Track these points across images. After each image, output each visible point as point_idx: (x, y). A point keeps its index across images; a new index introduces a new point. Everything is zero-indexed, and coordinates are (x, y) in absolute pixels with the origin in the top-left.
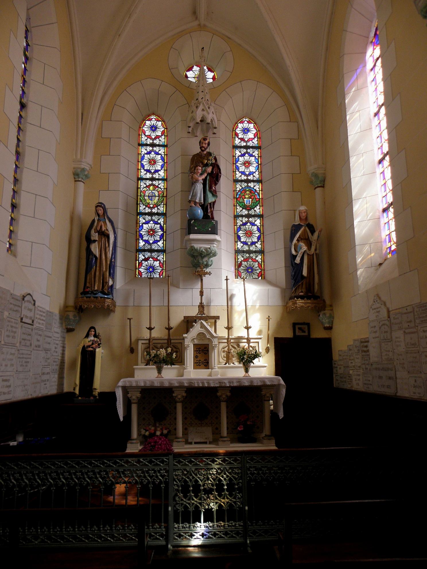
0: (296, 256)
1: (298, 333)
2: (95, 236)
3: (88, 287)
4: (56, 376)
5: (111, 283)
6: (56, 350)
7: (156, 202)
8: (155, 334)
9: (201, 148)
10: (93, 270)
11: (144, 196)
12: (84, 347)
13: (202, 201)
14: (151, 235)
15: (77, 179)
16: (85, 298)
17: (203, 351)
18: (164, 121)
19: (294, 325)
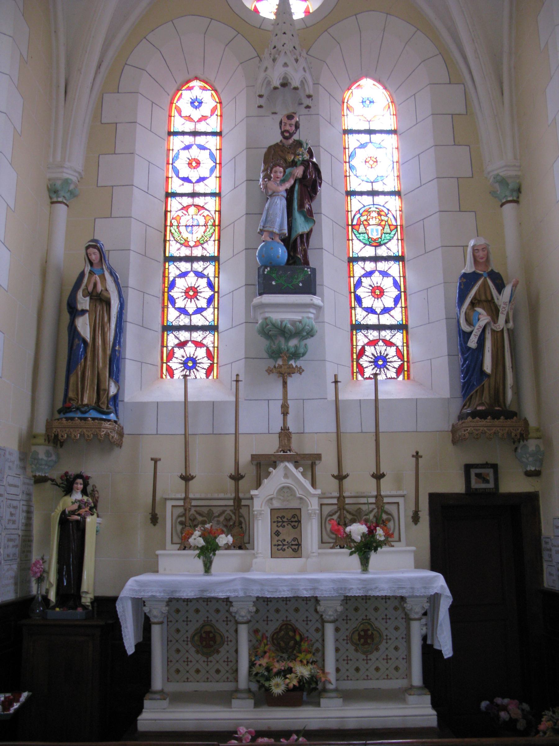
0: (471, 333)
1: (476, 484)
2: (84, 303)
3: (71, 399)
4: (15, 567)
5: (113, 390)
6: (13, 518)
7: (200, 237)
8: (197, 489)
9: (282, 133)
10: (79, 368)
11: (178, 227)
12: (64, 512)
13: (286, 231)
14: (191, 298)
15: (55, 200)
16: (64, 421)
17: (290, 522)
18: (216, 91)
19: (468, 468)
